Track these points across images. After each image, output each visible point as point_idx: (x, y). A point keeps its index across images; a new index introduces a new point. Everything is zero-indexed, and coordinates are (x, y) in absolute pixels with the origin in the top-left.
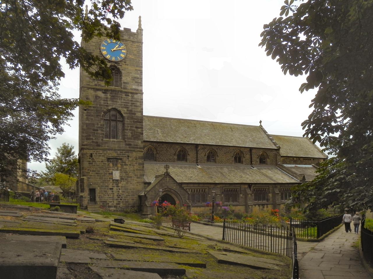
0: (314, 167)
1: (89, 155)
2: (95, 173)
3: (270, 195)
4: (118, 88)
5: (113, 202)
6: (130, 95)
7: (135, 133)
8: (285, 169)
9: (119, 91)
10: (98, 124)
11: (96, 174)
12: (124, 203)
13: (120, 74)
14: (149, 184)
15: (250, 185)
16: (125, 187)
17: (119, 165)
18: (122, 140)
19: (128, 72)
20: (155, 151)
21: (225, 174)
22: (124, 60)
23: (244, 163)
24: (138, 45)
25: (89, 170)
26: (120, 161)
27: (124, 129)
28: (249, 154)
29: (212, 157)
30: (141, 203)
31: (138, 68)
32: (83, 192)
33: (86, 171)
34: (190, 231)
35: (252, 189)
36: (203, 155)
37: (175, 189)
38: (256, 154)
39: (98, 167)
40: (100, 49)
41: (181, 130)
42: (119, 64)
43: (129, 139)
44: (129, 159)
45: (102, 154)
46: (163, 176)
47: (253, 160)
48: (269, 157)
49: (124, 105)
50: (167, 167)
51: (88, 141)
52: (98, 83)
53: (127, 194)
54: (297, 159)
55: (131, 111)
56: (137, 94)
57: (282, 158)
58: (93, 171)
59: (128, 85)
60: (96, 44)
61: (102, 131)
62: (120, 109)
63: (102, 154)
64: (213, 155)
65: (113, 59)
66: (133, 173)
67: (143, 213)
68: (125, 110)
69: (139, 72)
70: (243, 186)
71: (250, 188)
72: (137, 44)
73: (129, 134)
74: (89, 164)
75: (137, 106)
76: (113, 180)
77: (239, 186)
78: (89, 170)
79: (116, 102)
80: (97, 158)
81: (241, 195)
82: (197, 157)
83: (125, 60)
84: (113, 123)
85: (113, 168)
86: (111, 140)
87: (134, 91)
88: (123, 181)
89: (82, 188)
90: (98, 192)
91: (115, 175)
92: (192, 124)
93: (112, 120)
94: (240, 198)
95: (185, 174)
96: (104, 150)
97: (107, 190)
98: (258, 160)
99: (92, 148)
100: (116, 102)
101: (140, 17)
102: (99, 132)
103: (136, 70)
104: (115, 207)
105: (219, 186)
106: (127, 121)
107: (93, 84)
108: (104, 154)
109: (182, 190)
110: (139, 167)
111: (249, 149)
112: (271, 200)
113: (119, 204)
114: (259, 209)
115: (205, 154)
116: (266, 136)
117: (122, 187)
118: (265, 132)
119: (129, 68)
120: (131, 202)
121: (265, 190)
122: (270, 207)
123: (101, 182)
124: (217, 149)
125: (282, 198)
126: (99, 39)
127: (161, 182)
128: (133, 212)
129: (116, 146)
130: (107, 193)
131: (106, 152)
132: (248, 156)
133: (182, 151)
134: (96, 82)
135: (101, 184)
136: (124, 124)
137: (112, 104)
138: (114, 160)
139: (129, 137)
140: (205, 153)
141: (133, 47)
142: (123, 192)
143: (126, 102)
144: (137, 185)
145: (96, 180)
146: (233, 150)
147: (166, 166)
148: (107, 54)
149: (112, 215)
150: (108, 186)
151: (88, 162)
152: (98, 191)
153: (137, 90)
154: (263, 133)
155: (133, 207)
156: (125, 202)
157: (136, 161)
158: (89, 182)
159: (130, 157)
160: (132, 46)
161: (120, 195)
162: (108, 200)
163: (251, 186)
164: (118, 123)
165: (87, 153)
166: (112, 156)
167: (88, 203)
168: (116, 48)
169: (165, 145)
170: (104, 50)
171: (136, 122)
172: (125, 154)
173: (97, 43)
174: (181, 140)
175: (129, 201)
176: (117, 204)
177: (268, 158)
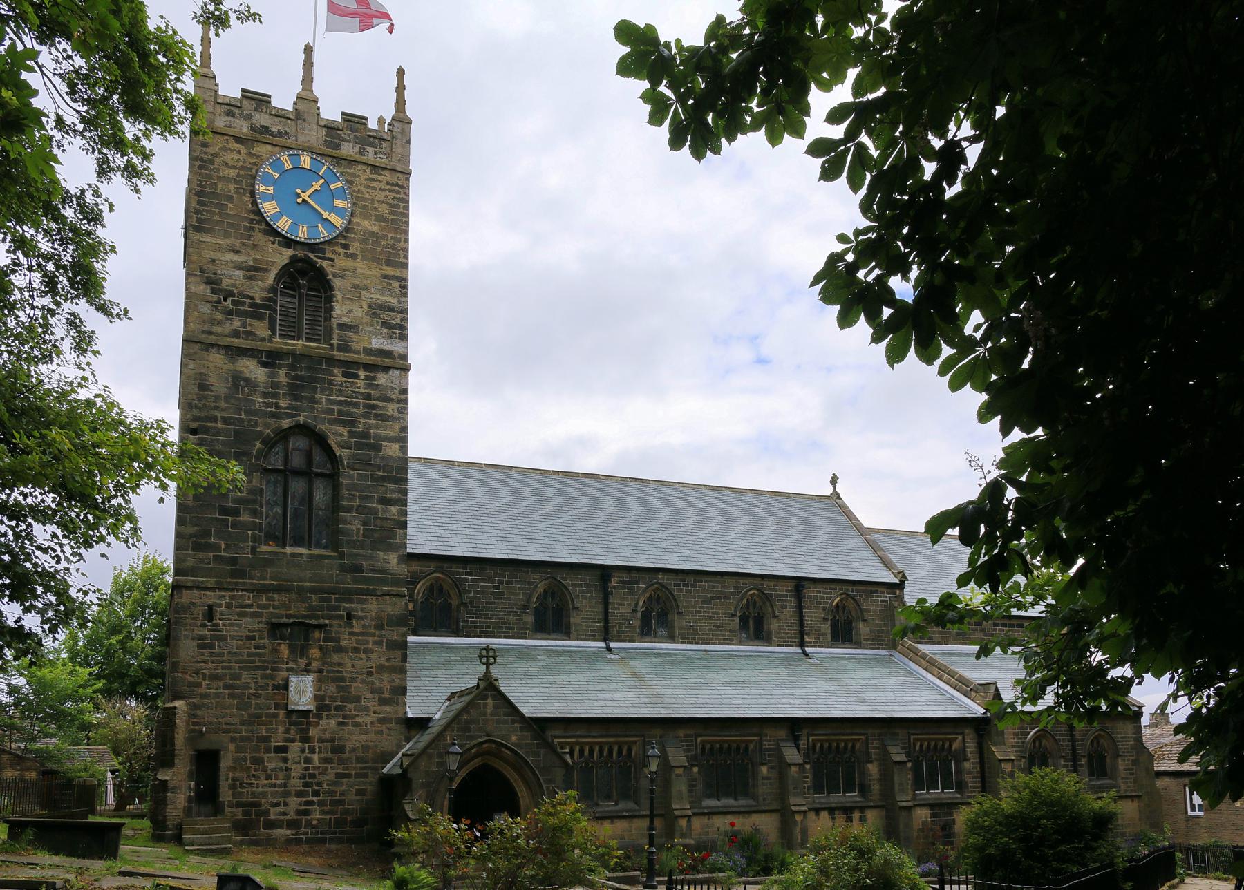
1: (199, 611)
2: (221, 683)
3: (873, 769)
5: (286, 804)
6: (362, 374)
15: (794, 725)
16: (332, 740)
17: (315, 652)
19: (357, 287)
20: (454, 594)
22: (342, 238)
24: (395, 180)
25: (197, 674)
28: (794, 603)
31: (390, 271)
36: (625, 609)
40: (253, 194)
42: (323, 251)
43: (354, 544)
45: (250, 606)
47: (807, 629)
48: (866, 617)
51: (201, 555)
52: (244, 325)
55: (365, 435)
56: (386, 369)
58: (214, 677)
60: (238, 175)
62: (323, 427)
63: (250, 606)
65: (302, 233)
68: (343, 430)
69: (396, 285)
72: (387, 177)
76: (290, 713)
81: (764, 769)
83: (345, 238)
84: (297, 486)
85: (291, 665)
86: (289, 550)
91: (297, 691)
94: (760, 782)
99: (211, 582)
102: (245, 518)
103: (385, 277)
104: (292, 824)
106: (349, 477)
107: (227, 331)
108: (259, 606)
109: (542, 751)
112: (876, 788)
113: (306, 813)
117: (321, 740)
118: (849, 515)
119: (359, 270)
123: (242, 723)
124: (676, 585)
126: (250, 154)
130: (265, 769)
132: (788, 614)
134: (237, 323)
136: (336, 488)
138: (296, 633)
141: (374, 188)
144: (380, 733)
148: (280, 214)
150: (267, 739)
151: (195, 643)
152: (225, 763)
153: (388, 354)
158: (195, 724)
159: (359, 618)
161: (312, 776)
162: (264, 795)
165: (193, 604)
166: (288, 616)
167: (188, 811)
171: (383, 479)
172: (338, 608)
176: (299, 813)
177: (864, 621)
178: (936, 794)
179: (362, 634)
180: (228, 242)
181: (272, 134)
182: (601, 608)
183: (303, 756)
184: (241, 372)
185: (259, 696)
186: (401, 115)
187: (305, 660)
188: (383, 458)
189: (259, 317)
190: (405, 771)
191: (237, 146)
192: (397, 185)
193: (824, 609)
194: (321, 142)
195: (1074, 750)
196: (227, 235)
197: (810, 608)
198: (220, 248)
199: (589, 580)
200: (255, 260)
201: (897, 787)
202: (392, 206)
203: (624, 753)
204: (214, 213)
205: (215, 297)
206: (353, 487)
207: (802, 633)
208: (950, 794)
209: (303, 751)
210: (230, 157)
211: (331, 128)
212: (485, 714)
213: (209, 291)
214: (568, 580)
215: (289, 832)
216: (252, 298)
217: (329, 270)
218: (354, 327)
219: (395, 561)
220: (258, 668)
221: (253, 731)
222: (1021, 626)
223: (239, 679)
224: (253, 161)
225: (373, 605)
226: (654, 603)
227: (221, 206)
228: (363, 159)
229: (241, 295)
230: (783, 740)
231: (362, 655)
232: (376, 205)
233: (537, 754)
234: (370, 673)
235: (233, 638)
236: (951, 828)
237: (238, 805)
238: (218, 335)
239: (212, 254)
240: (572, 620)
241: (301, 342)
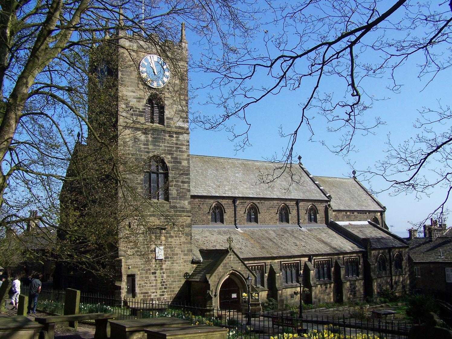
5: (156, 292)
6: (175, 136)
7: (181, 190)
12: (169, 293)
16: (170, 269)
17: (163, 238)
47: (300, 218)
55: (176, 158)
68: (169, 157)
75: (182, 152)
79: (159, 146)
87: (180, 130)
98: (306, 217)
100: (159, 146)
113: (163, 295)
117: (166, 269)
123: (142, 264)
142: (168, 276)
152: (137, 279)
161: (164, 282)
171: (182, 174)
174: (216, 192)
188: (182, 166)
192: (184, 66)
199: (230, 201)
200: (140, 95)
214: (223, 202)
216: (139, 109)
219: (187, 204)
231: (178, 238)
237: (142, 293)
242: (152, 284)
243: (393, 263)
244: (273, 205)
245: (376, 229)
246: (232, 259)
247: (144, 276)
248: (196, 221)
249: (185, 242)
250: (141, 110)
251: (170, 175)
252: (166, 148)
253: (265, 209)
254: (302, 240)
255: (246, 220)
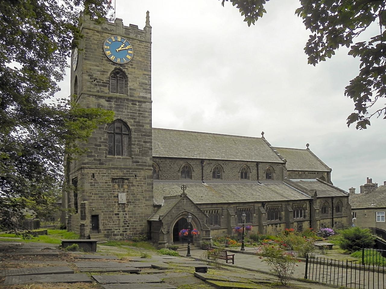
0: (319, 181)
1: (90, 175)
2: (98, 196)
3: (283, 213)
4: (123, 96)
5: (119, 229)
6: (137, 104)
7: (143, 148)
8: (293, 185)
9: (124, 99)
10: (100, 138)
11: (99, 197)
12: (132, 230)
13: (125, 79)
14: (159, 206)
15: (263, 203)
16: (132, 211)
17: (126, 186)
18: (128, 157)
19: (135, 77)
20: (162, 167)
21: (234, 192)
22: (131, 62)
23: (250, 179)
24: (147, 45)
25: (90, 193)
26: (126, 181)
27: (130, 144)
28: (256, 168)
29: (218, 173)
30: (150, 229)
31: (146, 73)
32: (85, 219)
33: (88, 194)
34: (233, 264)
35: (265, 207)
36: (208, 171)
37: (192, 212)
38: (263, 168)
39: (102, 189)
40: (103, 48)
41: (183, 143)
42: (125, 66)
43: (136, 155)
44: (136, 178)
45: (105, 173)
46: (180, 198)
47: (259, 176)
48: (275, 172)
49: (131, 116)
50: (184, 188)
51: (90, 158)
52: (101, 89)
53: (135, 220)
54: (302, 173)
55: (139, 122)
56: (145, 102)
57: (288, 173)
58: (96, 194)
59: (135, 92)
60: (98, 43)
61: (106, 146)
62: (126, 120)
63: (105, 173)
64: (218, 171)
65: (118, 61)
66: (142, 195)
67: (159, 242)
68: (132, 121)
69: (147, 77)
70: (256, 205)
71: (264, 207)
72: (145, 44)
73: (136, 150)
74: (91, 185)
75: (145, 117)
76: (119, 204)
77: (253, 205)
78: (90, 193)
79: (122, 112)
80: (100, 179)
81: (255, 215)
82: (202, 174)
83: (132, 62)
84: (117, 137)
85: (119, 190)
86: (116, 157)
87: (142, 100)
88: (130, 205)
89: (83, 214)
90: (102, 218)
91: (121, 198)
92: (193, 136)
93: (117, 134)
94: (254, 218)
95: (202, 193)
96: (108, 169)
97: (112, 216)
98: (265, 175)
99: (94, 166)
100: (122, 112)
101: (148, 12)
102: (102, 147)
103: (144, 74)
104: (121, 235)
105: (232, 206)
106: (134, 135)
107: (95, 91)
108: (108, 173)
109: (200, 214)
110: (148, 188)
111: (255, 163)
112: (284, 218)
113: (126, 231)
114: (272, 229)
115: (210, 170)
116: (270, 148)
117: (128, 211)
118: (268, 145)
119: (136, 72)
120: (139, 229)
121: (278, 208)
122: (283, 226)
123: (105, 207)
124: (223, 164)
125: (294, 217)
126: (102, 36)
127: (178, 205)
128: (142, 240)
129: (122, 165)
130: (112, 220)
131: (111, 171)
132: (254, 172)
133: (187, 167)
134: (98, 88)
135: (106, 209)
136: (130, 138)
137: (117, 114)
138: (120, 181)
139: (136, 153)
140: (210, 169)
141: (140, 47)
142: (130, 217)
143: (133, 113)
144: (146, 209)
145: (100, 205)
146: (240, 165)
147: (183, 187)
148: (111, 55)
149: (122, 246)
150: (113, 211)
151: (90, 184)
152: (101, 218)
153: (145, 98)
154: (266, 145)
155: (141, 234)
156: (133, 229)
157: (144, 180)
158: (91, 207)
159: (138, 176)
160: (140, 46)
161: (127, 221)
162: (113, 227)
163: (265, 204)
164: (123, 136)
165: (88, 173)
166: (117, 176)
167: (90, 232)
168: (121, 47)
169: (168, 161)
170: (108, 50)
171: (145, 135)
172: (132, 174)
173: (99, 41)
174: (186, 155)
175: (137, 227)
176: (123, 232)
177: (275, 173)
178: (299, 219)
179: (140, 181)
180: (95, 63)
181: (108, 30)
182: (201, 171)
183: (124, 216)
184: (100, 103)
185: (110, 199)
186: (148, 26)
187: (123, 189)
188: (145, 129)
189: (105, 86)
190: (160, 221)
191: (98, 34)
192: (147, 46)
193: (264, 170)
194: (124, 33)
195: (333, 206)
196: (95, 61)
197: (260, 170)
198: (93, 65)
199: (198, 162)
200: (104, 69)
201: (290, 218)
202: (146, 53)
203: (216, 212)
204: (91, 54)
205: (91, 80)
206: (135, 138)
207: (258, 177)
208: (302, 219)
209: (124, 215)
210: (95, 37)
211: (126, 28)
212: (184, 204)
213: (89, 78)
214: (192, 163)
215: (121, 237)
216: (103, 81)
217: (126, 72)
218: (134, 90)
219: (149, 160)
220: (109, 191)
221: (108, 209)
222: (315, 173)
223: (103, 194)
224: (102, 38)
225: (143, 172)
226: (217, 169)
227: (92, 52)
228: (137, 38)
229: (99, 79)
230: (260, 207)
231: (140, 187)
232: (141, 52)
233: (199, 215)
234: (142, 192)
235: (101, 183)
236: (302, 227)
237: (105, 230)
238: (92, 92)
239: (89, 67)
240: (192, 174)
241: (118, 94)
242: (115, 223)
243: (335, 208)
244: (236, 166)
245: (322, 184)
246: (185, 203)
247: (107, 216)
248: (168, 177)
249: (146, 190)
250: (105, 81)
251: (133, 136)
252: (129, 114)
253: (229, 169)
254: (258, 191)
255: (212, 177)
